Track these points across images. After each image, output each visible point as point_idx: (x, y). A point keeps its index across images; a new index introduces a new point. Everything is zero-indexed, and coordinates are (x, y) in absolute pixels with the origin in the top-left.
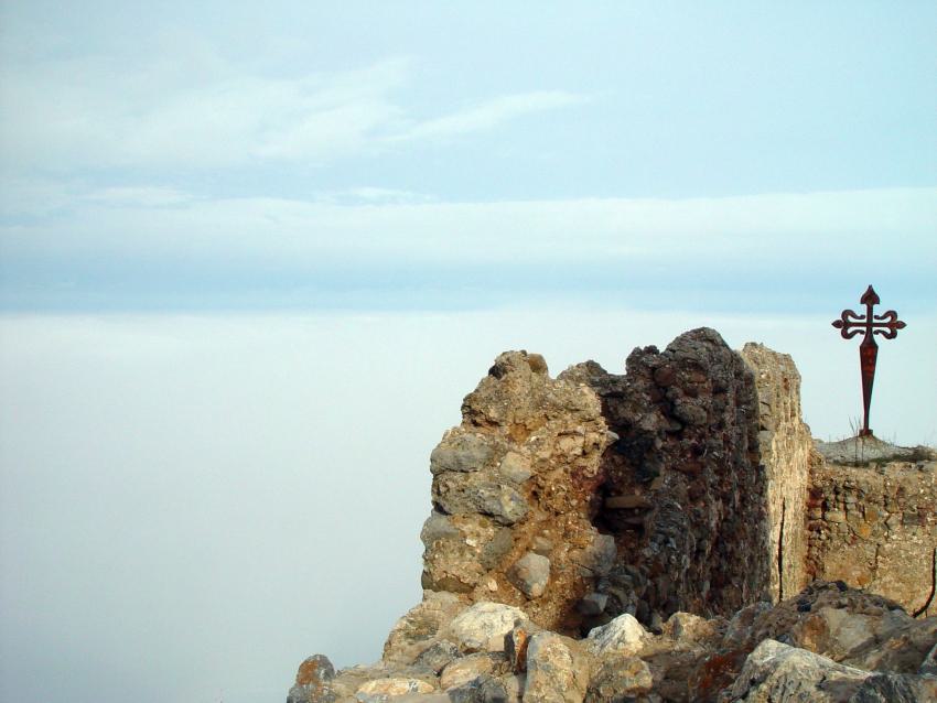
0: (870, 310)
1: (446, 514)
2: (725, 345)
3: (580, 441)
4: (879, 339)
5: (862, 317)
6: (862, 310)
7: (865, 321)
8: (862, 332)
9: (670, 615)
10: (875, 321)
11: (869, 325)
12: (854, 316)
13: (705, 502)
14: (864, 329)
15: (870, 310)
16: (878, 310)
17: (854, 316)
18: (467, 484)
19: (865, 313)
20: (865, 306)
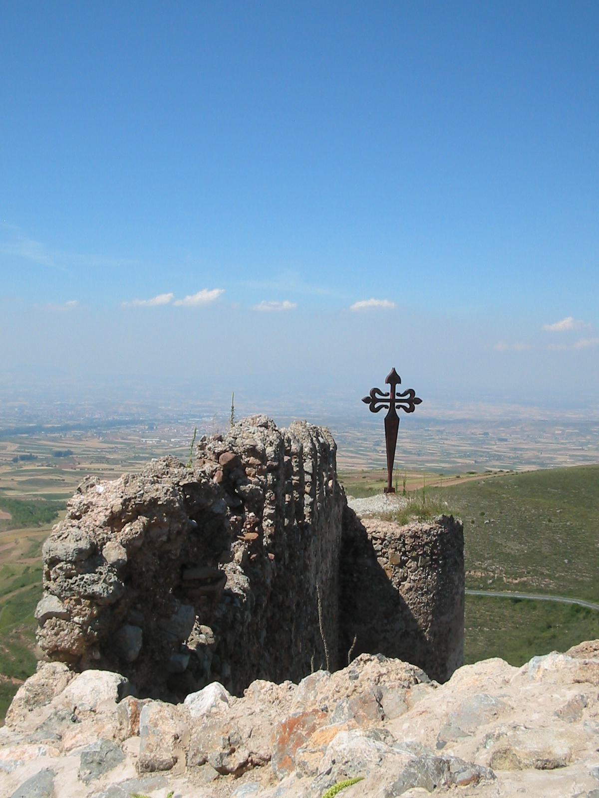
4: (400, 412)
6: (386, 388)
8: (386, 407)
16: (400, 389)
17: (380, 393)
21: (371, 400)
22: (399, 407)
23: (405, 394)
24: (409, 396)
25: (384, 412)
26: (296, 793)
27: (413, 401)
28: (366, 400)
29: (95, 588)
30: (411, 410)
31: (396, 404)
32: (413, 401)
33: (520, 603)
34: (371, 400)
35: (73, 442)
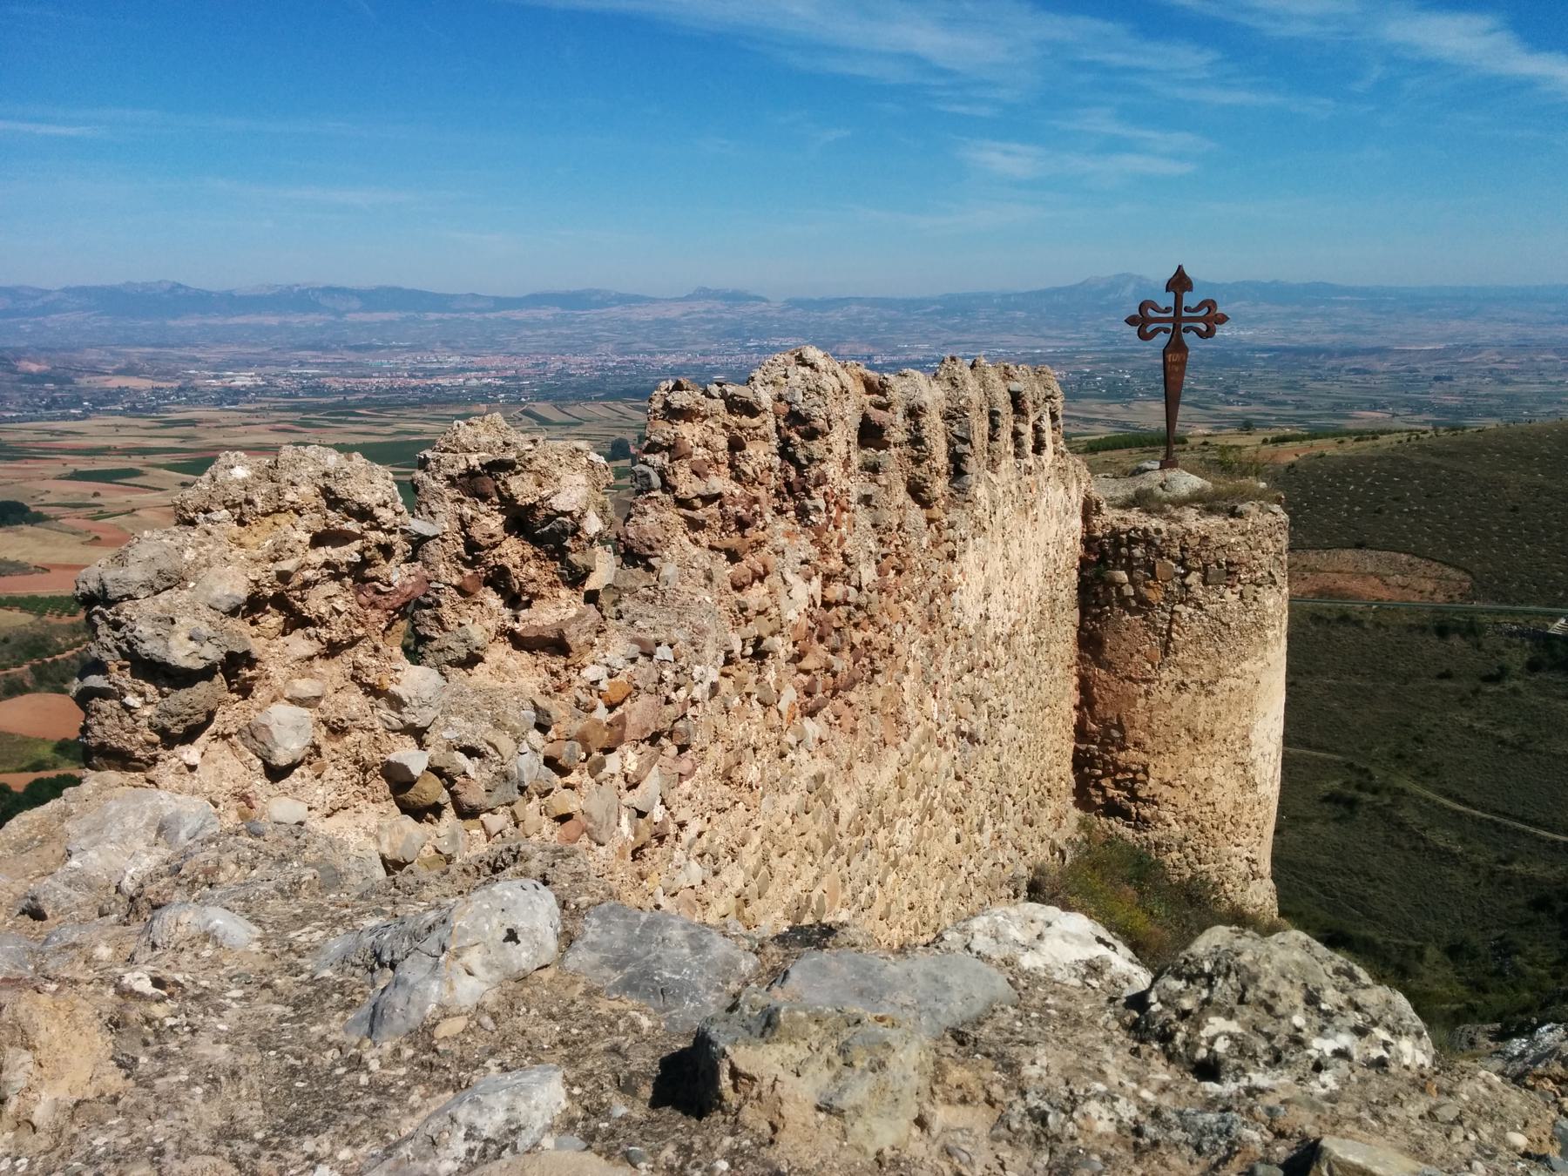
0: (1178, 300)
1: (1326, 800)
2: (209, 294)
3: (357, 544)
4: (1190, 338)
5: (1167, 310)
6: (1168, 300)
7: (1171, 314)
8: (1166, 331)
9: (721, 1097)
10: (1185, 314)
11: (1177, 319)
12: (1156, 309)
13: (798, 919)
14: (1185, 314)
15: (1178, 300)
16: (1190, 300)
17: (1156, 309)
18: (973, 1034)
19: (1172, 304)
20: (1172, 295)
21: (1141, 321)
22: (1186, 330)
23: (1156, 331)
24: (1205, 310)
25: (1162, 339)
26: (385, 505)
27: (1212, 318)
28: (1131, 321)
29: (554, 613)
30: (1209, 333)
31: (1184, 325)
32: (1212, 318)
33: (297, 694)
34: (1141, 321)
35: (19, 473)
